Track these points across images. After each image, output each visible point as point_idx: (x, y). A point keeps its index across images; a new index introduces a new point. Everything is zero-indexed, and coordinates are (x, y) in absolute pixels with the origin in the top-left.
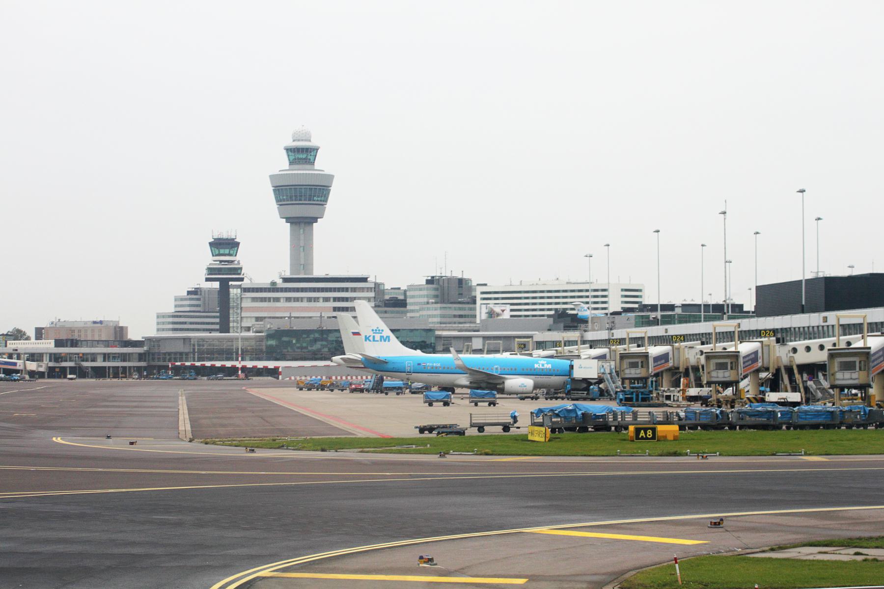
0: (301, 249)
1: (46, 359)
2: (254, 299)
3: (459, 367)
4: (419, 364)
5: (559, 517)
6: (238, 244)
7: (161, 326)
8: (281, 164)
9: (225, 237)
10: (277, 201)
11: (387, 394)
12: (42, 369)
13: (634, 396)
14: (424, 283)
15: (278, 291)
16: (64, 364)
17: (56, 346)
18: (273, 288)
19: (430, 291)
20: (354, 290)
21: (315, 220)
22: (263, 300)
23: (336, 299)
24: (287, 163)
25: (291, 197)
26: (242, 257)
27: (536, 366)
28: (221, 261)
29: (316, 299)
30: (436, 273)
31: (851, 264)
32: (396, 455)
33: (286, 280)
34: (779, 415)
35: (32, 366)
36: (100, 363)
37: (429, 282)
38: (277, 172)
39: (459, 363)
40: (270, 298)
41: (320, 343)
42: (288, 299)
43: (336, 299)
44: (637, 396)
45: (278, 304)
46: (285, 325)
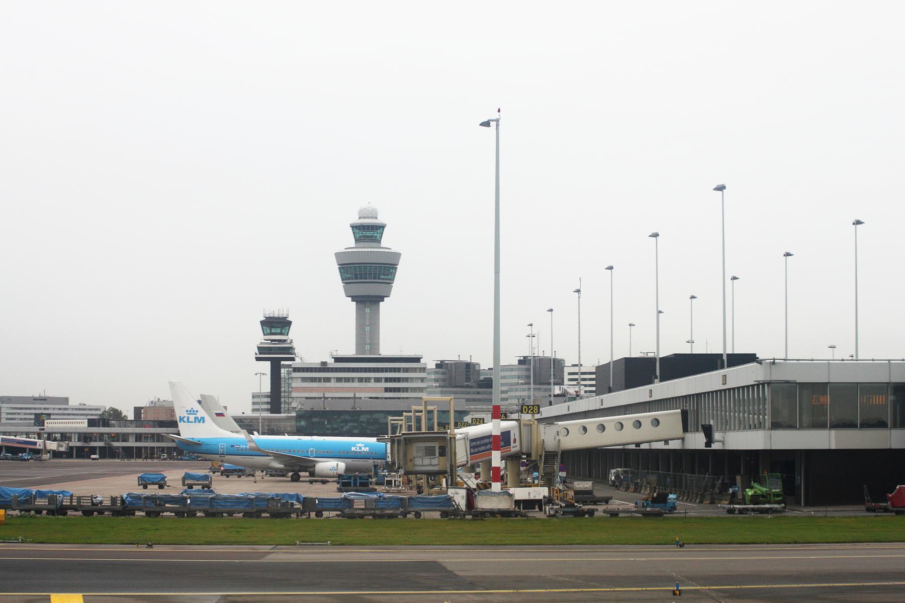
0: (367, 328)
1: (75, 438)
2: (304, 380)
3: (251, 449)
4: (233, 446)
6: (290, 323)
7: (257, 407)
8: (347, 241)
9: (276, 315)
10: (343, 280)
11: (228, 476)
12: (62, 449)
13: (352, 481)
14: (517, 363)
16: (93, 444)
17: (89, 426)
18: (324, 368)
20: (407, 370)
21: (381, 298)
22: (313, 380)
23: (387, 380)
26: (295, 336)
27: (353, 449)
28: (272, 340)
29: (367, 380)
31: (832, 344)
33: (337, 360)
34: (189, 501)
35: (52, 446)
36: (132, 443)
37: (520, 362)
39: (253, 445)
41: (350, 424)
42: (339, 380)
43: (387, 380)
44: (355, 480)
45: (328, 385)
46: (318, 406)
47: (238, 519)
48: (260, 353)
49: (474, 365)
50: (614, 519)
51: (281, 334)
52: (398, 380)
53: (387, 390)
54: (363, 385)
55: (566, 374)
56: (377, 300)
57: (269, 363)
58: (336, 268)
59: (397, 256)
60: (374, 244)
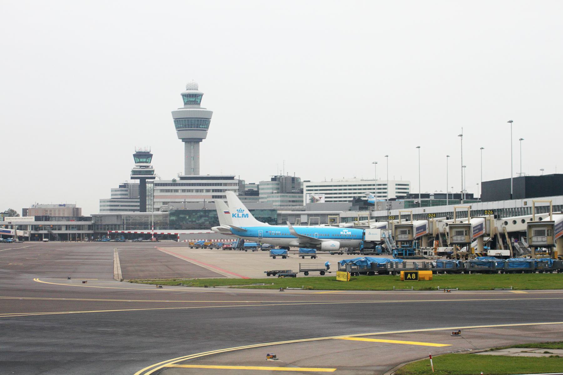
0: (192, 158)
1: (29, 229)
2: (162, 191)
3: (292, 234)
4: (267, 232)
5: (356, 329)
6: (151, 155)
7: (103, 208)
8: (179, 104)
9: (143, 151)
10: (177, 128)
11: (246, 251)
12: (27, 235)
13: (404, 252)
14: (270, 180)
15: (177, 186)
16: (41, 232)
17: (36, 220)
18: (174, 183)
19: (274, 185)
20: (225, 184)
21: (200, 140)
22: (168, 191)
23: (214, 191)
24: (183, 104)
25: (185, 126)
26: (154, 164)
27: (341, 233)
28: (141, 166)
29: (201, 191)
30: (278, 174)
31: (542, 168)
32: (252, 290)
33: (182, 178)
34: (496, 264)
35: (20, 233)
36: (63, 231)
37: (273, 179)
38: (176, 110)
39: (293, 231)
40: (172, 190)
41: (204, 218)
42: (184, 191)
43: (214, 191)
44: (406, 252)
45: (177, 194)
46: (181, 207)
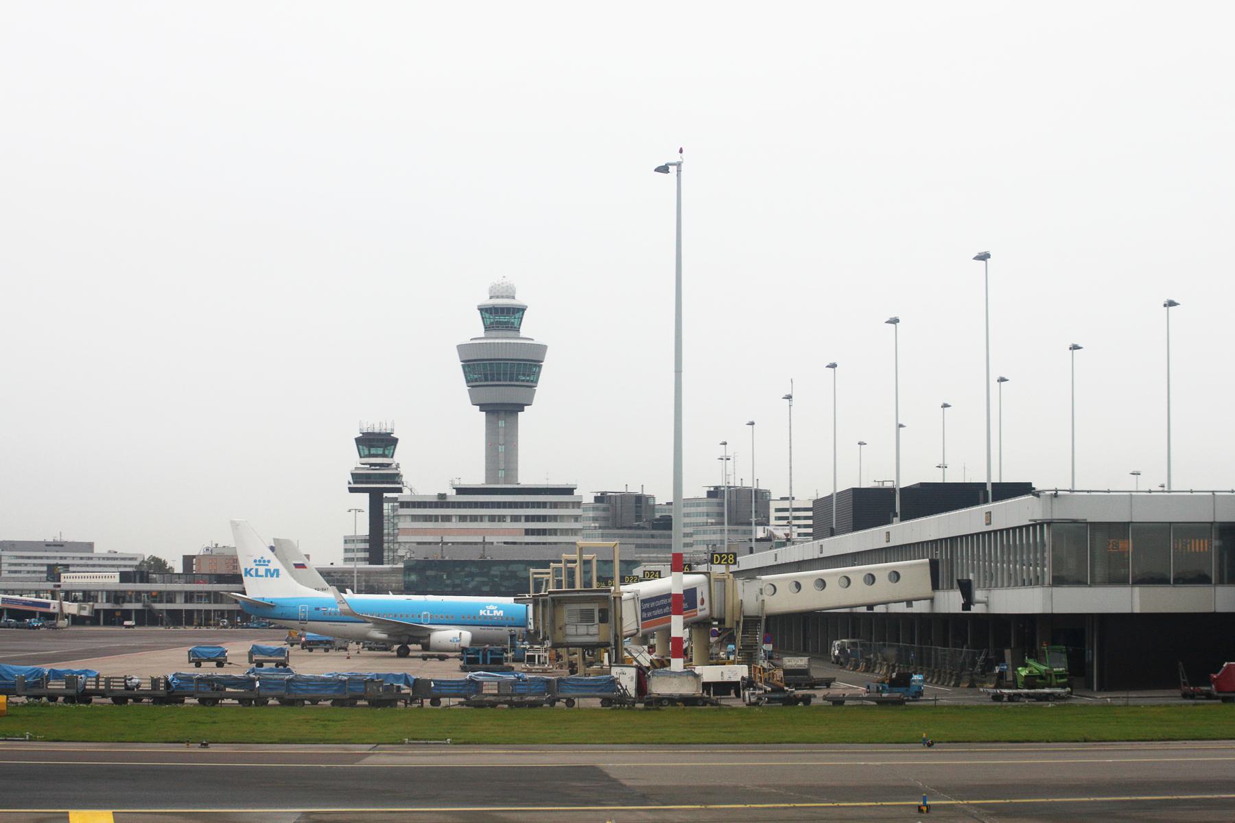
0: (501, 448)
1: (102, 598)
2: (415, 518)
3: (343, 613)
4: (317, 609)
6: (395, 441)
7: (350, 555)
8: (474, 329)
9: (377, 430)
10: (468, 381)
11: (311, 650)
12: (85, 613)
13: (480, 656)
14: (705, 496)
16: (127, 606)
17: (121, 581)
18: (442, 502)
20: (555, 505)
21: (520, 407)
22: (427, 518)
23: (529, 518)
26: (402, 458)
27: (482, 612)
28: (371, 465)
29: (502, 518)
31: (1136, 469)
33: (460, 491)
34: (258, 684)
35: (71, 608)
36: (180, 605)
37: (710, 494)
39: (345, 607)
41: (478, 579)
42: (463, 518)
43: (529, 518)
44: (485, 655)
45: (447, 525)
46: (434, 554)
47: (325, 708)
48: (355, 482)
49: (647, 498)
50: (838, 708)
51: (384, 455)
52: (543, 518)
53: (528, 532)
54: (496, 525)
55: (772, 511)
56: (514, 409)
57: (367, 495)
58: (458, 366)
59: (542, 349)
60: (511, 333)
